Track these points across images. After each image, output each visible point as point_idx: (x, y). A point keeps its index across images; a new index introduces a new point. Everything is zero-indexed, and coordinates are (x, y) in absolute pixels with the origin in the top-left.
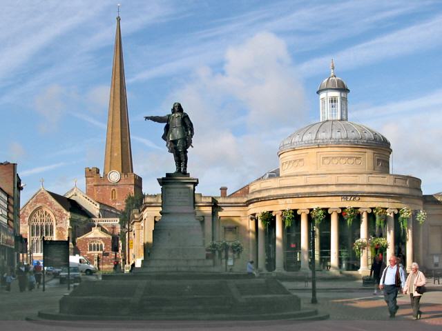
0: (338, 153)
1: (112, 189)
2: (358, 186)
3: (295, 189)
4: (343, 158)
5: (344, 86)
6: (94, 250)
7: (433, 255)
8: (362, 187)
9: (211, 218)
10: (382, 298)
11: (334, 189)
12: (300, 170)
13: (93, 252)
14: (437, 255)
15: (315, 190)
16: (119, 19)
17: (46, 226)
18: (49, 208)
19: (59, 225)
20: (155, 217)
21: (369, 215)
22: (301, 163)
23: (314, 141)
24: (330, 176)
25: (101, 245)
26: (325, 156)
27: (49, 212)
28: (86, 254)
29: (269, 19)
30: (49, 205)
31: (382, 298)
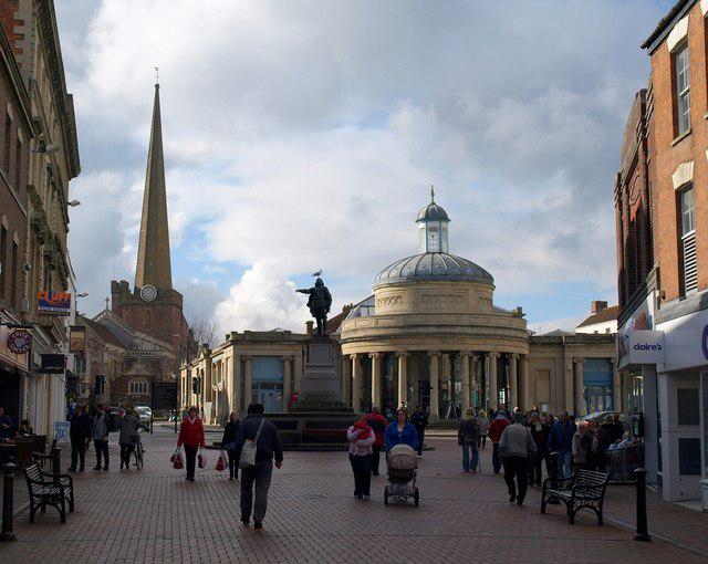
11: (434, 330)
15: (414, 330)
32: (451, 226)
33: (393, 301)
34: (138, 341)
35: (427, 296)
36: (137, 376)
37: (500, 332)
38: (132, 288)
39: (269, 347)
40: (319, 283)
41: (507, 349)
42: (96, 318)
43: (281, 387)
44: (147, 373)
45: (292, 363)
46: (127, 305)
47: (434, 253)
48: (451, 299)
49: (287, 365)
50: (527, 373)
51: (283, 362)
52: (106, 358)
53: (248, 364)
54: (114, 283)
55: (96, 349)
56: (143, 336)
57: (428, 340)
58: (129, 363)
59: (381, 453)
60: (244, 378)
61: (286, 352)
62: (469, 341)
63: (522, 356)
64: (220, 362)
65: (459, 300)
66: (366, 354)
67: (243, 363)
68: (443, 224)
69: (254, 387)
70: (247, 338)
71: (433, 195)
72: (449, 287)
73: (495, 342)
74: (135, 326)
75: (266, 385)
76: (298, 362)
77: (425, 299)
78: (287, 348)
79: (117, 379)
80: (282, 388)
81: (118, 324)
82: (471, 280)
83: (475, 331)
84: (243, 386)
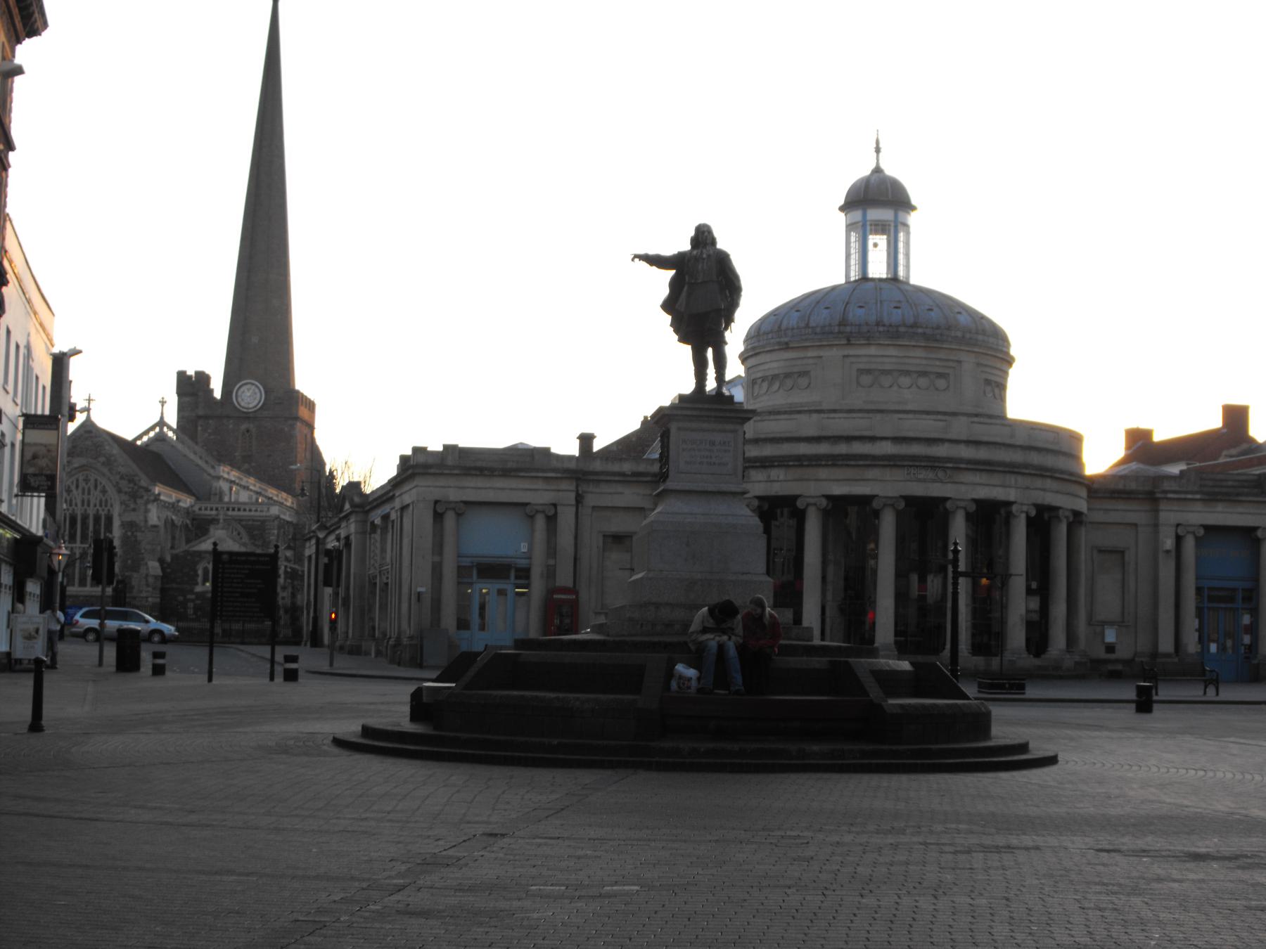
0: (894, 360)
1: (244, 427)
2: (946, 445)
4: (907, 373)
7: (1104, 624)
9: (574, 509)
10: (42, 496)
11: (887, 448)
12: (800, 398)
14: (1111, 623)
15: (842, 449)
17: (97, 519)
18: (105, 470)
19: (129, 517)
20: (436, 502)
21: (1030, 522)
22: (803, 381)
23: (836, 329)
24: (879, 416)
26: (862, 366)
28: (192, 592)
30: (103, 464)
31: (42, 496)
34: (224, 486)
35: (869, 371)
40: (703, 237)
42: (140, 437)
43: (524, 574)
45: (552, 520)
46: (206, 417)
48: (923, 382)
49: (540, 522)
50: (1083, 557)
51: (531, 517)
52: (154, 516)
53: (450, 520)
54: (182, 376)
55: (134, 496)
56: (234, 475)
58: (200, 526)
60: (441, 553)
61: (538, 494)
63: (1077, 514)
64: (386, 517)
65: (941, 383)
69: (462, 571)
70: (450, 462)
71: (878, 150)
72: (919, 353)
73: (1026, 481)
74: (223, 455)
75: (492, 570)
76: (566, 518)
77: (866, 379)
78: (540, 485)
79: (174, 557)
80: (528, 577)
81: (193, 456)
83: (983, 454)
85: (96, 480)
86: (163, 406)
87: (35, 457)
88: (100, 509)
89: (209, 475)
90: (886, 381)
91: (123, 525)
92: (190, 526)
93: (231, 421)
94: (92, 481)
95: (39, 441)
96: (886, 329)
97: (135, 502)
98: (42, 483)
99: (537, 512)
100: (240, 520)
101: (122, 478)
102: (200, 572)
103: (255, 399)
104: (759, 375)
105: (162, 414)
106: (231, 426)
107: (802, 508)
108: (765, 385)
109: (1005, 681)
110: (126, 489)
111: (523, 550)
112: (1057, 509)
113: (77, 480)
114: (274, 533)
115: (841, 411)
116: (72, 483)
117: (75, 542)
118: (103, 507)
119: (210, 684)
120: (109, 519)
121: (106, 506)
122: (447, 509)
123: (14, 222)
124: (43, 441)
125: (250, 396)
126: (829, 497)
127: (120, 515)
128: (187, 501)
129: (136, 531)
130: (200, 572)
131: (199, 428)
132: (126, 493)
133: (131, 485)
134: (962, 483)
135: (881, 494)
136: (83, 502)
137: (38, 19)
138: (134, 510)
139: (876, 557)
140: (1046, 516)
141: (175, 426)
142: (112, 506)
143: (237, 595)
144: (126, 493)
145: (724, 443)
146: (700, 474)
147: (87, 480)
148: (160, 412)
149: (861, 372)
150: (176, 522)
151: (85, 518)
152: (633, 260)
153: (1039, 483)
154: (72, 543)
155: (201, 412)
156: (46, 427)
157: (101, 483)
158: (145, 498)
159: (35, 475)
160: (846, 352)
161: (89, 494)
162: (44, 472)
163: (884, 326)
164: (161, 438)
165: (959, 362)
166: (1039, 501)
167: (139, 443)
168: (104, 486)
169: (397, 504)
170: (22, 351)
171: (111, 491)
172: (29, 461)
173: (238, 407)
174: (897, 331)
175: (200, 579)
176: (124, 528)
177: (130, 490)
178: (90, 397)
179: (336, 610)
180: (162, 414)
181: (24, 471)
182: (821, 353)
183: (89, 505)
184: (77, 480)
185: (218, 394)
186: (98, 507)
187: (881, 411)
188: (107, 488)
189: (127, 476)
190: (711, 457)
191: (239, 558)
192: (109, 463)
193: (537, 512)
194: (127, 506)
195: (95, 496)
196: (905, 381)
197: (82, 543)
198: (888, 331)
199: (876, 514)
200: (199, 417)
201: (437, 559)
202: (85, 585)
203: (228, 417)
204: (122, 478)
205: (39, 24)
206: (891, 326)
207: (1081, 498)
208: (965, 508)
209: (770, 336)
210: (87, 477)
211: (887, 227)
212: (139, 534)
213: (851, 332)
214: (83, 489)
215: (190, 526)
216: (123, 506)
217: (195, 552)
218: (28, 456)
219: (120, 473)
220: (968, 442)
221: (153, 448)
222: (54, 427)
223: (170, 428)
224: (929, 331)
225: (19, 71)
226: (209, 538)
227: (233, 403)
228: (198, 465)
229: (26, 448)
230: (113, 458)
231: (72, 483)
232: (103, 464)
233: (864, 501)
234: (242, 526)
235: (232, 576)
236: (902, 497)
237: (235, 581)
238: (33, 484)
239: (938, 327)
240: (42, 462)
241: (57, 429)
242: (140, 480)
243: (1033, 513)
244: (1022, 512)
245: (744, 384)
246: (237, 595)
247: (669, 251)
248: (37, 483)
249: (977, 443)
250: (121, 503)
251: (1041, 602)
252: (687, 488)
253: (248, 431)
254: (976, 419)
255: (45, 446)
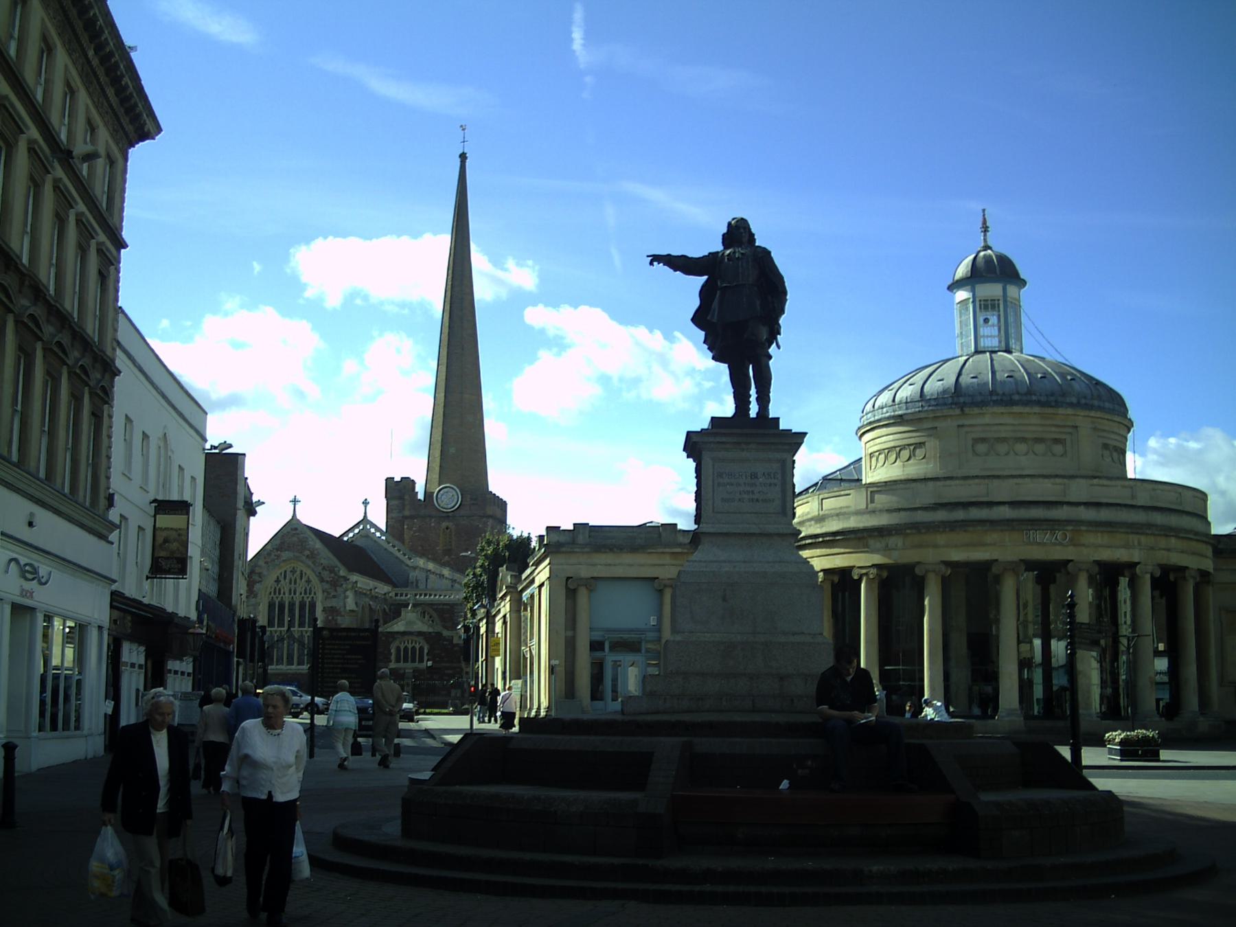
1: (444, 524)
3: (833, 552)
4: (1023, 440)
5: (191, 482)
6: (406, 660)
8: (1074, 509)
11: (1005, 512)
13: (401, 665)
16: (463, 157)
17: (302, 605)
19: (329, 604)
20: (568, 578)
21: (1156, 583)
23: (950, 400)
25: (421, 649)
27: (309, 572)
29: (78, 169)
32: (1027, 297)
33: (905, 454)
35: (983, 440)
36: (404, 633)
37: (1158, 518)
38: (420, 489)
39: (628, 558)
40: (738, 233)
41: (1176, 559)
44: (425, 628)
46: (412, 517)
47: (992, 352)
48: (1040, 448)
50: (1211, 616)
51: (660, 592)
53: (583, 596)
54: (389, 481)
57: (993, 537)
59: (422, 498)
62: (1090, 538)
65: (1058, 449)
66: (844, 572)
67: (571, 594)
68: (1012, 290)
69: (596, 646)
71: (985, 229)
77: (982, 448)
78: (667, 559)
82: (1083, 404)
83: (1105, 515)
84: (571, 645)
85: (302, 571)
86: (366, 507)
87: (166, 541)
88: (275, 597)
89: (407, 565)
90: (1002, 448)
91: (324, 610)
92: (387, 610)
93: (433, 520)
94: (298, 572)
95: (170, 526)
96: (999, 398)
97: (336, 591)
98: (172, 566)
99: (665, 586)
100: (431, 605)
101: (324, 568)
102: (393, 651)
103: (453, 501)
104: (875, 448)
105: (365, 513)
106: (433, 524)
107: (921, 574)
108: (882, 457)
109: (1138, 748)
110: (328, 579)
111: (652, 624)
112: (1184, 569)
113: (285, 572)
114: (461, 616)
115: (957, 478)
116: (281, 574)
117: (274, 627)
118: (308, 595)
119: (312, 759)
120: (313, 606)
121: (280, 594)
122: (578, 585)
123: (127, 311)
124: (175, 526)
125: (449, 499)
126: (947, 564)
127: (322, 602)
128: (383, 589)
129: (337, 616)
130: (393, 651)
131: (405, 527)
132: (327, 582)
133: (333, 575)
134: (1084, 545)
135: (1001, 558)
136: (290, 590)
137: (147, 122)
138: (334, 597)
139: (997, 621)
140: (1172, 578)
141: (384, 528)
142: (315, 594)
143: (338, 671)
144: (327, 582)
145: (769, 474)
146: (740, 513)
147: (293, 571)
148: (364, 511)
149: (977, 441)
150: (373, 607)
151: (292, 605)
152: (651, 263)
153: (1163, 542)
154: (281, 627)
155: (407, 513)
156: (177, 512)
157: (306, 574)
158: (344, 586)
159: (167, 558)
160: (960, 422)
161: (295, 583)
162: (175, 555)
163: (998, 395)
164: (365, 535)
165: (1076, 427)
166: (1164, 562)
167: (345, 539)
168: (308, 577)
169: (537, 584)
170: (154, 443)
171: (315, 581)
172: (161, 546)
173: (438, 507)
174: (1011, 399)
175: (393, 657)
176: (326, 613)
177: (331, 579)
178: (295, 499)
179: (475, 683)
180: (365, 513)
181: (156, 555)
182: (936, 424)
183: (295, 594)
184: (285, 572)
185: (421, 496)
186: (303, 595)
187: (998, 477)
188: (311, 578)
189: (328, 567)
190: (753, 492)
191: (340, 634)
192: (313, 556)
193: (665, 586)
194: (329, 593)
195: (301, 586)
196: (1022, 447)
197: (299, 627)
198: (1002, 400)
199: (998, 579)
200: (405, 518)
201: (570, 633)
202: (407, 662)
203: (431, 517)
204: (324, 568)
205: (149, 126)
206: (1004, 394)
207: (1207, 557)
208: (1088, 571)
209: (885, 410)
210: (294, 568)
211: (996, 302)
212: (339, 618)
213: (964, 403)
214: (291, 580)
215: (387, 610)
216: (325, 594)
217: (389, 632)
218: (160, 540)
219: (322, 564)
220: (1087, 504)
221: (358, 543)
222: (184, 512)
223: (378, 529)
224: (1043, 399)
225: (688, 457)
226: (401, 620)
227: (434, 505)
228: (397, 558)
229: (158, 533)
230: (316, 552)
231: (281, 574)
232: (308, 556)
233: (984, 567)
234: (434, 610)
235: (333, 651)
236: (1021, 560)
237: (336, 656)
238: (164, 567)
239: (1052, 394)
240: (174, 546)
241: (188, 514)
242: (339, 571)
243: (1158, 573)
244: (1146, 573)
245: (1162, 704)
246: (338, 671)
247: (697, 251)
248: (168, 566)
249: (1098, 505)
250: (323, 592)
251: (978, 716)
252: (725, 531)
253: (447, 528)
254: (1095, 481)
255: (176, 530)
